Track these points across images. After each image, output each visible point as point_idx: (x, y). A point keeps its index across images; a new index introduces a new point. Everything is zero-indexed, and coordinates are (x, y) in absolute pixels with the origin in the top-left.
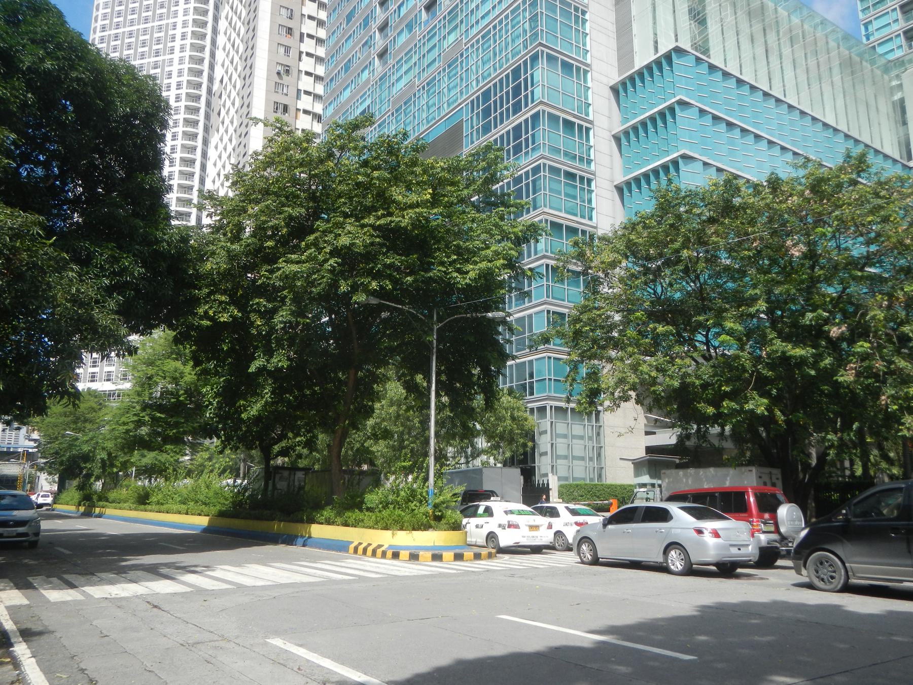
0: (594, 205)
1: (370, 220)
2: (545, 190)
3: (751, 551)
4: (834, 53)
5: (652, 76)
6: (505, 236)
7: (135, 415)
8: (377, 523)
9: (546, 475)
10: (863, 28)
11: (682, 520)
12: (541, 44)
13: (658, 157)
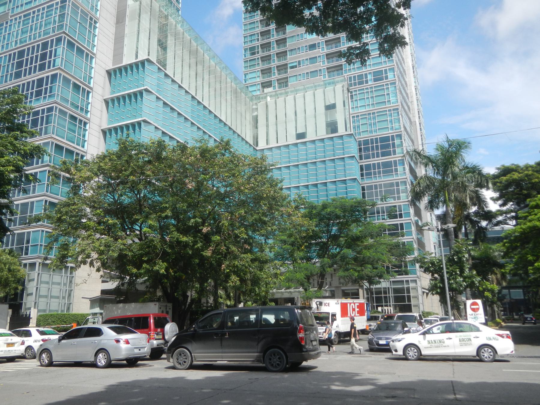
0: (86, 139)
2: (54, 123)
3: (146, 350)
4: (229, 85)
5: (126, 73)
6: (16, 150)
9: (30, 309)
10: (244, 76)
11: (108, 333)
12: (64, 33)
13: (129, 118)
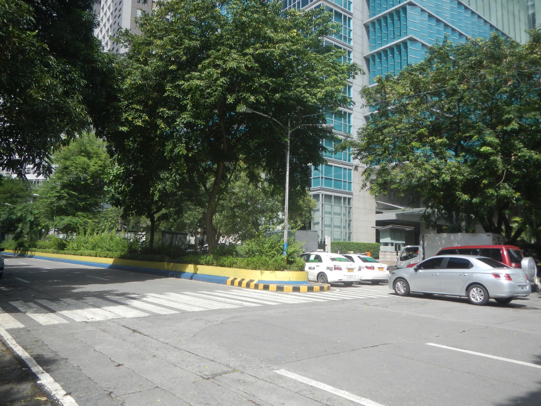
1: (250, 51)
7: (57, 192)
8: (248, 265)
